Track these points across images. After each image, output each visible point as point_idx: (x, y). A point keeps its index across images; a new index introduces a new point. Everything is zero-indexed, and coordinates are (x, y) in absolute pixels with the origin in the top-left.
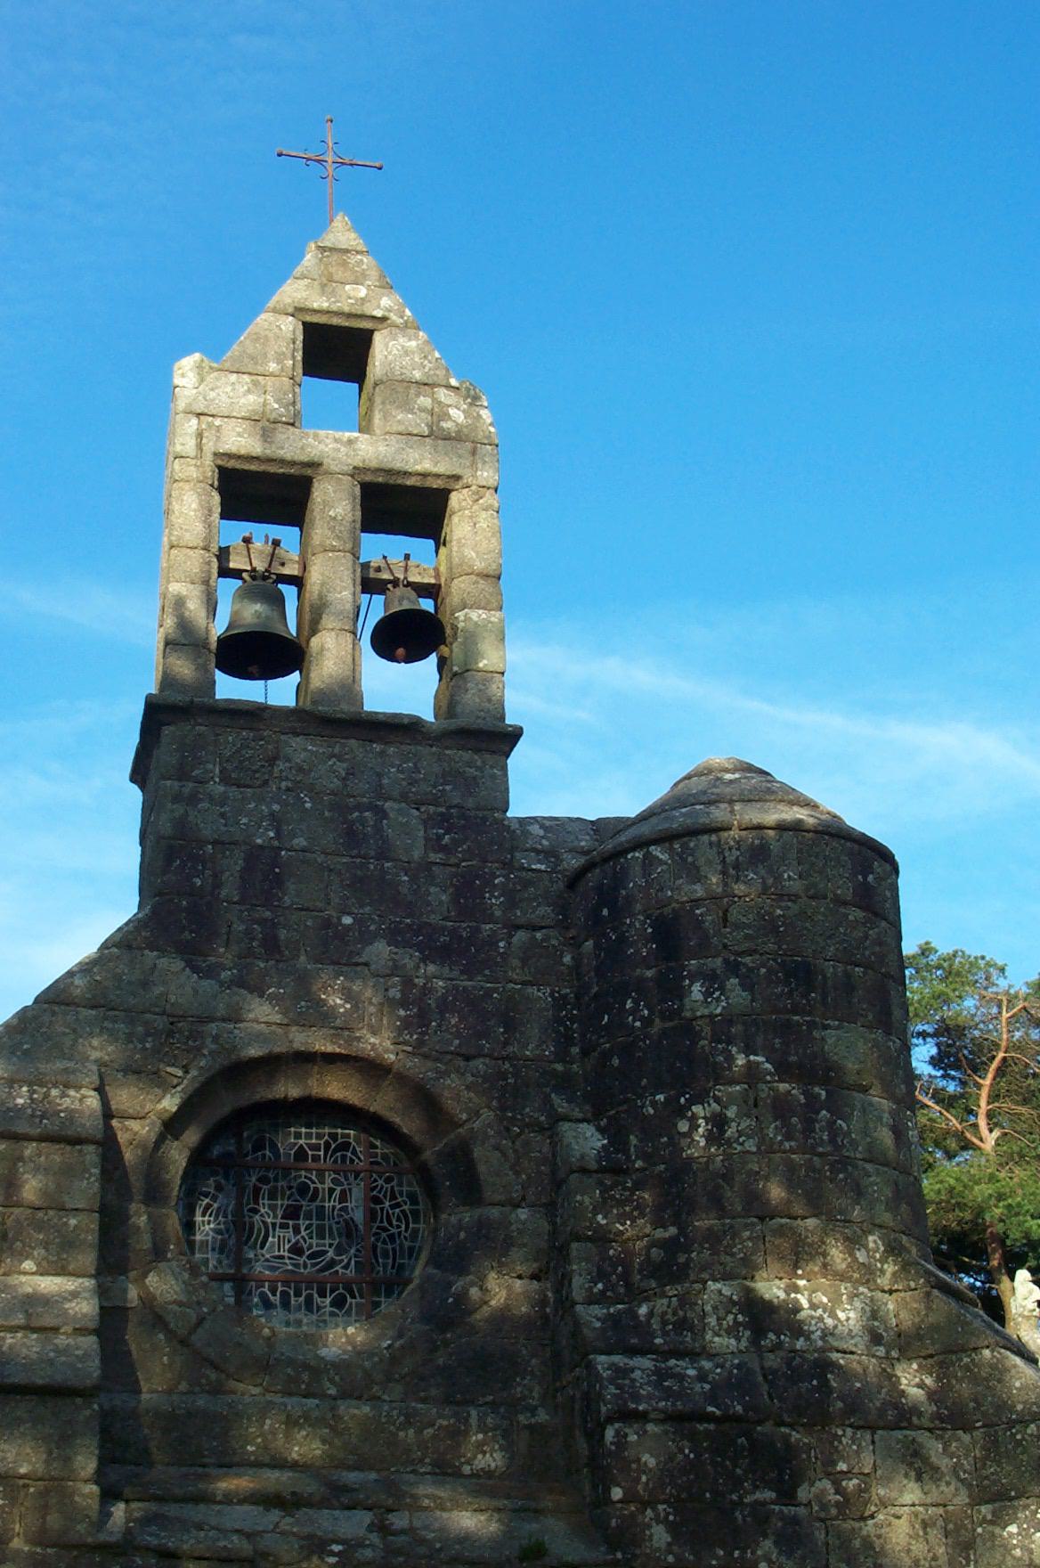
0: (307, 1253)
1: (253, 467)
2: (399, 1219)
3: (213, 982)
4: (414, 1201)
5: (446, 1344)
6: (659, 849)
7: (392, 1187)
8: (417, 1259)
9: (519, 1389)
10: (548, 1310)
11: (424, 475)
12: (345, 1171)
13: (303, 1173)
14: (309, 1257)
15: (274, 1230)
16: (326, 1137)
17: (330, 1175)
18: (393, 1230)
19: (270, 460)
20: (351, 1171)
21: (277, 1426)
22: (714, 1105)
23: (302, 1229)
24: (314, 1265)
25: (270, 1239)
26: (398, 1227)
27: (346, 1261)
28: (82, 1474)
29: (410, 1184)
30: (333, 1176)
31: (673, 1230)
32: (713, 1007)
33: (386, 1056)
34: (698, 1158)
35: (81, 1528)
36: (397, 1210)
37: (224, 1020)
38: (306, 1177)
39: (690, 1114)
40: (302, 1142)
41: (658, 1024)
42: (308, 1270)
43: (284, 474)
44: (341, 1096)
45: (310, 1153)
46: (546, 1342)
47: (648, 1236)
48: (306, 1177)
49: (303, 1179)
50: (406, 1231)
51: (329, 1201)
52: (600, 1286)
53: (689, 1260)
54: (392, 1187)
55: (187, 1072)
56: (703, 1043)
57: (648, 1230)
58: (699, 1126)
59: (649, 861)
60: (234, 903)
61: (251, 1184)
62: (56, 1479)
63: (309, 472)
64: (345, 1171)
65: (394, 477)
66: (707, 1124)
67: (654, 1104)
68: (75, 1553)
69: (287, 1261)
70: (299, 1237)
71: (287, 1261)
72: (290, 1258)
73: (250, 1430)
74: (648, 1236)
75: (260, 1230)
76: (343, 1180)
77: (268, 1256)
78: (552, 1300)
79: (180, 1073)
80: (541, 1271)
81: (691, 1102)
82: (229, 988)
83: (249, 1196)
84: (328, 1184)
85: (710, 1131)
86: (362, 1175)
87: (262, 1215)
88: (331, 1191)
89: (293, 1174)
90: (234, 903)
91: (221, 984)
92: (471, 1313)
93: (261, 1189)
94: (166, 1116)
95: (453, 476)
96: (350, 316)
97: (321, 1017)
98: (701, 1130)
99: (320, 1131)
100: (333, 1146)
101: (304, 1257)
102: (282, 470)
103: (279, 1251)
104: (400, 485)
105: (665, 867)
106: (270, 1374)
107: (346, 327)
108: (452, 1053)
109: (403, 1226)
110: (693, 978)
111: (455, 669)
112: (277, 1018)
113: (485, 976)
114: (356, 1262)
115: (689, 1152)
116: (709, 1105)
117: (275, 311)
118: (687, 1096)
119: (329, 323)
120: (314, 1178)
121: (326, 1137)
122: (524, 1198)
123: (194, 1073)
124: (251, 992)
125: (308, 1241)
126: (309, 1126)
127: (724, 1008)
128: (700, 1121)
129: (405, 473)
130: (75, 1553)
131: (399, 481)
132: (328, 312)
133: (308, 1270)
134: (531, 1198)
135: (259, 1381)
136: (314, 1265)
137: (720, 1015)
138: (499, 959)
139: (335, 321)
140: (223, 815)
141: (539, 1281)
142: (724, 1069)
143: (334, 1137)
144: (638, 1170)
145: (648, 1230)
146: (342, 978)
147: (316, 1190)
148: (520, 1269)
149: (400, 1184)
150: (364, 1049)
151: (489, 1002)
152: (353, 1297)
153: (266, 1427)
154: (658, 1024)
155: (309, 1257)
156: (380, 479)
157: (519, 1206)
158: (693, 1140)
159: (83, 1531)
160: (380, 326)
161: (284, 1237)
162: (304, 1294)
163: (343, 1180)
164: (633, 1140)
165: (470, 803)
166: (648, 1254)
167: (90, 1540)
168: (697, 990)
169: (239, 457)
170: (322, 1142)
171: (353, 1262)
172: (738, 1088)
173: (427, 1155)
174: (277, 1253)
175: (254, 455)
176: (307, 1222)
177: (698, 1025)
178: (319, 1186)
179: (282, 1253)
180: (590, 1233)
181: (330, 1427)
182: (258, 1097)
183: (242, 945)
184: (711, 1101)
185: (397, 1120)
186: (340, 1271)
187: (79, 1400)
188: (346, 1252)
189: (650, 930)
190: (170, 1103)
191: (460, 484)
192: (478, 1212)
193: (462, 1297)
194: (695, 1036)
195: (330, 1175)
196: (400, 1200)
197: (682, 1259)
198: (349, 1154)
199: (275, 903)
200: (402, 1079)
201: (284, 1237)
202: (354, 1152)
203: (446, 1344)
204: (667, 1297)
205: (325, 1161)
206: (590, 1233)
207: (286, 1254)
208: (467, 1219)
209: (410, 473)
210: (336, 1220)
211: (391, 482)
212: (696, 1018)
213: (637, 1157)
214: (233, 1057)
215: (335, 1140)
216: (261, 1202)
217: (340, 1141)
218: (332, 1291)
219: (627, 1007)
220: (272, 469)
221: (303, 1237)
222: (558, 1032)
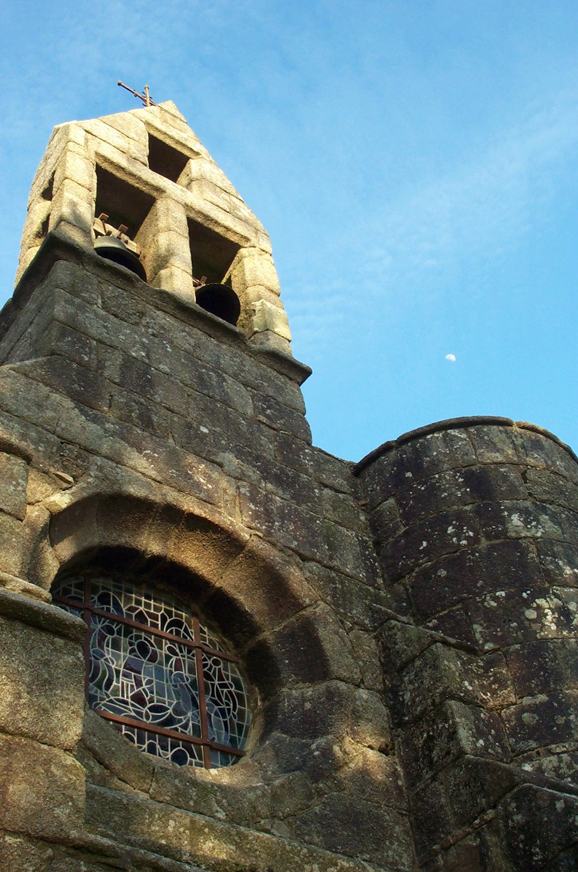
0: (149, 705)
1: (119, 175)
2: (227, 698)
3: (99, 427)
4: (238, 687)
5: (320, 793)
6: (457, 431)
7: (219, 669)
8: (246, 736)
9: (390, 853)
10: (400, 783)
11: (228, 229)
12: (180, 644)
13: (143, 634)
14: (151, 709)
15: (118, 677)
16: (163, 611)
17: (166, 644)
18: (224, 706)
19: (131, 174)
20: (185, 645)
21: (182, 830)
22: (556, 600)
23: (144, 683)
24: (155, 718)
25: (114, 683)
26: (227, 704)
27: (184, 721)
28: (62, 738)
29: (233, 672)
30: (169, 645)
31: (542, 698)
32: (533, 530)
33: (242, 534)
34: (552, 639)
35: (62, 813)
36: (225, 690)
37: (106, 457)
38: (145, 639)
39: (535, 605)
40: (142, 608)
41: (484, 543)
42: (150, 721)
43: (138, 188)
44: (193, 565)
45: (149, 620)
46: (404, 812)
47: (515, 704)
48: (145, 639)
49: (143, 640)
50: (234, 709)
51: (166, 666)
52: (481, 742)
53: (568, 722)
54: (219, 669)
55: (76, 481)
56: (531, 555)
57: (513, 699)
58: (547, 614)
59: (449, 441)
60: (115, 383)
61: (97, 630)
62: (23, 735)
63: (155, 194)
64: (180, 644)
65: (209, 222)
66: (553, 613)
67: (496, 599)
68: (50, 852)
69: (130, 707)
70: (141, 689)
71: (130, 707)
72: (133, 705)
73: (153, 828)
74: (515, 704)
75: (104, 673)
76: (178, 651)
77: (112, 698)
78: (402, 774)
79: (71, 479)
80: (387, 746)
81: (533, 597)
82: (112, 436)
83: (94, 639)
84: (165, 651)
85: (558, 619)
86: (194, 651)
87: (106, 660)
88: (168, 658)
89: (134, 633)
90: (115, 383)
91: (106, 431)
92: (338, 768)
93: (107, 636)
94: (55, 509)
95: (245, 238)
96: (178, 142)
97: (187, 485)
98: (549, 618)
99: (158, 604)
100: (169, 620)
101: (146, 708)
102: (137, 185)
103: (123, 696)
104: (210, 229)
105: (464, 442)
106: (157, 782)
107: (173, 148)
108: (292, 550)
109: (232, 705)
110: (511, 511)
111: (256, 329)
112: (153, 473)
113: (308, 506)
114: (193, 724)
115: (542, 634)
116: (552, 600)
117: (133, 114)
118: (529, 592)
119: (164, 141)
120: (152, 641)
121: (163, 611)
122: (362, 681)
123: (82, 484)
124: (132, 446)
125: (149, 695)
126: (148, 597)
127: (542, 533)
128: (546, 611)
129: (216, 222)
130: (50, 852)
131: (211, 226)
132: (165, 133)
133: (150, 721)
134: (368, 682)
135: (146, 786)
136: (155, 718)
137: (541, 537)
138: (316, 499)
139: (168, 141)
140: (106, 327)
141: (387, 755)
142: (556, 575)
143: (170, 613)
144: (488, 651)
145: (513, 699)
146: (203, 466)
147: (155, 653)
148: (370, 741)
149: (226, 669)
150: (225, 522)
151: (314, 524)
152: (193, 756)
153: (170, 829)
154: (484, 543)
155: (151, 709)
156: (199, 220)
157: (359, 687)
158: (544, 625)
159: (64, 819)
160: (194, 157)
161: (127, 685)
162: (147, 743)
163: (178, 651)
164: (477, 628)
165: (280, 399)
166: (519, 719)
167: (74, 834)
168: (516, 519)
169: (112, 163)
170: (159, 614)
171: (190, 725)
172: (572, 590)
173: (267, 635)
174: (120, 697)
175: (122, 166)
176: (148, 678)
177: (524, 543)
178: (158, 650)
179: (125, 698)
180: (462, 695)
181: (237, 844)
182: (123, 540)
183: (123, 412)
184: (553, 597)
185: (241, 598)
186: (180, 729)
187: (60, 642)
188: (185, 714)
189: (461, 480)
190: (62, 500)
191: (249, 244)
192: (322, 687)
193: (327, 752)
194: (524, 552)
195: (166, 644)
196: (226, 682)
197: (561, 720)
198: (182, 631)
199: (148, 396)
200: (253, 557)
201: (127, 685)
202: (186, 630)
203: (320, 793)
204: (554, 754)
205: (162, 629)
206: (462, 695)
207: (129, 700)
208: (310, 693)
209: (219, 224)
210: (173, 683)
211: (206, 225)
212: (521, 538)
213: (486, 641)
214: (116, 487)
215: (171, 617)
216: (105, 648)
217: (174, 618)
218: (173, 747)
219: (449, 532)
220: (132, 181)
221: (144, 689)
222: (366, 564)
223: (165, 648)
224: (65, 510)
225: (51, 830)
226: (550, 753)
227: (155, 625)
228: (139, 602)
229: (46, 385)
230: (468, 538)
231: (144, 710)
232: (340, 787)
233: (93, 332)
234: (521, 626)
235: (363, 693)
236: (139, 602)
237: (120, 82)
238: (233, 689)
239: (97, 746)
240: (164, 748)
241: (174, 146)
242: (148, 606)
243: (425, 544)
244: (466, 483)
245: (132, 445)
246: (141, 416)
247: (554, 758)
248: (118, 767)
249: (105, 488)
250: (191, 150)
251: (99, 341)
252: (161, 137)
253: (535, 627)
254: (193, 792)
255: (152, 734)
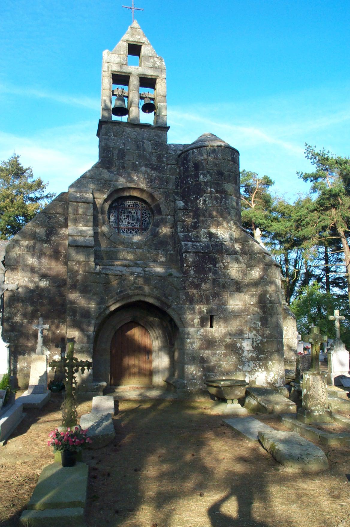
11: (152, 76)
14: (131, 224)
35: (92, 270)
40: (129, 204)
41: (194, 183)
53: (199, 225)
59: (193, 152)
63: (129, 75)
81: (200, 197)
88: (135, 212)
91: (114, 174)
96: (137, 42)
97: (132, 181)
98: (201, 202)
110: (201, 174)
117: (122, 41)
123: (109, 191)
126: (130, 201)
139: (134, 43)
143: (135, 203)
148: (168, 227)
154: (194, 183)
165: (160, 141)
190: (105, 196)
197: (197, 225)
200: (147, 192)
203: (155, 239)
223: (134, 210)
224: (106, 198)
225: (91, 272)
226: (194, 231)
227: (132, 207)
228: (128, 202)
229: (101, 168)
230: (191, 182)
231: (129, 225)
232: (160, 237)
233: (111, 146)
234: (196, 204)
235: (169, 217)
236: (128, 202)
237: (122, 6)
238: (148, 216)
239: (114, 241)
240: (133, 231)
241: (136, 44)
242: (130, 202)
243: (185, 182)
244: (194, 167)
245: (120, 176)
246: (122, 167)
247: (194, 233)
248: (117, 244)
249: (115, 189)
250: (142, 43)
251: (113, 148)
252: (132, 43)
253: (199, 204)
254: (130, 245)
255: (131, 229)
